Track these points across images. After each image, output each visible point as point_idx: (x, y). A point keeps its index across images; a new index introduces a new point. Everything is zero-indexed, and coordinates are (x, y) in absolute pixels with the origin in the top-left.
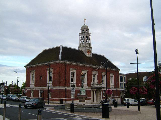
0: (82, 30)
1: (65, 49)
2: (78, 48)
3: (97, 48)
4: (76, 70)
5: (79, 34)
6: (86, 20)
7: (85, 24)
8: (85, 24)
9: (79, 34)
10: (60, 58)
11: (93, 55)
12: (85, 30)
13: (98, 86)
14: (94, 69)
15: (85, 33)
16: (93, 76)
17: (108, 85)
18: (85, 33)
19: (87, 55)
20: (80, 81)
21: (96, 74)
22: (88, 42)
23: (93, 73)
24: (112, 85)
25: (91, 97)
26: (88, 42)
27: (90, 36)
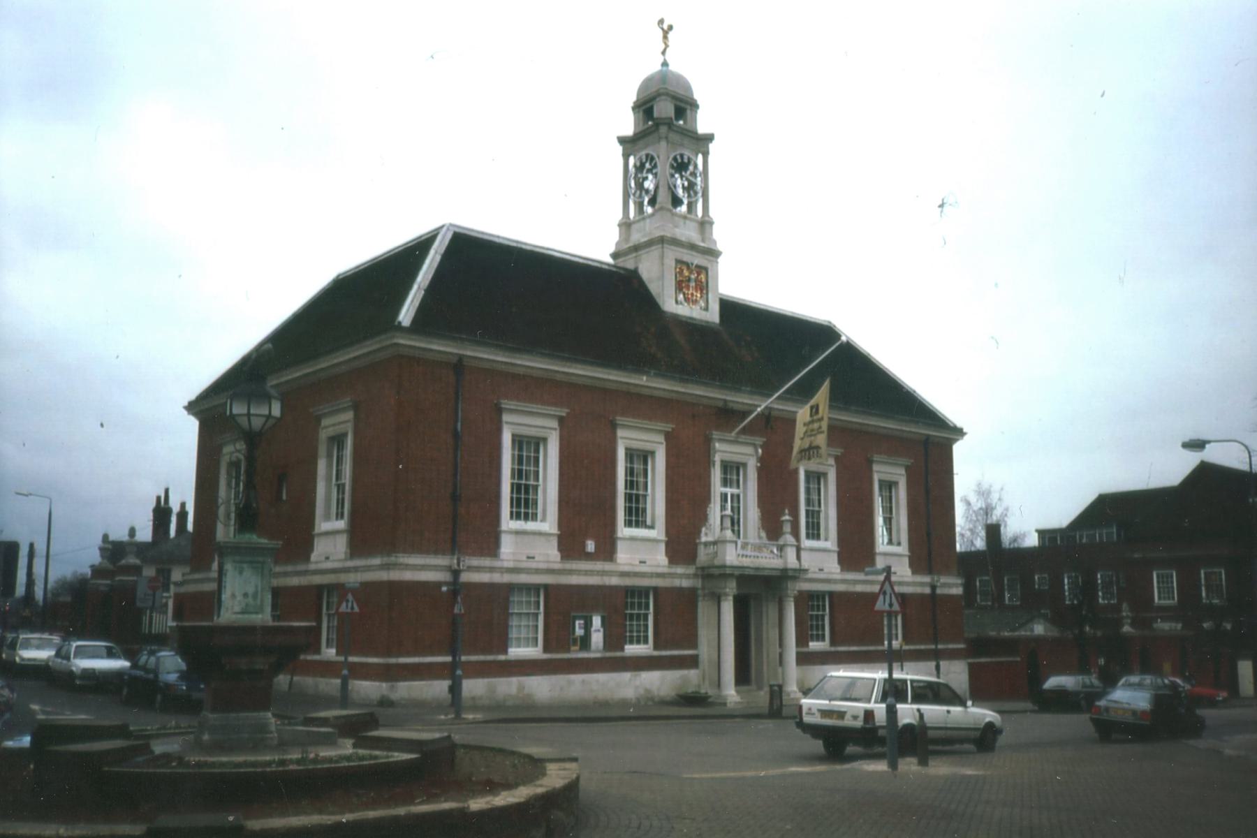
0: (644, 107)
1: (467, 249)
2: (615, 256)
3: (763, 258)
4: (561, 420)
5: (622, 140)
6: (670, 28)
7: (665, 64)
8: (665, 64)
9: (622, 140)
10: (406, 315)
11: (730, 308)
12: (664, 109)
13: (768, 560)
14: (727, 417)
15: (665, 126)
16: (716, 474)
17: (856, 549)
18: (665, 126)
19: (672, 304)
20: (587, 522)
21: (748, 454)
22: (691, 206)
23: (724, 450)
24: (812, 550)
25: (694, 645)
26: (691, 206)
27: (706, 155)
